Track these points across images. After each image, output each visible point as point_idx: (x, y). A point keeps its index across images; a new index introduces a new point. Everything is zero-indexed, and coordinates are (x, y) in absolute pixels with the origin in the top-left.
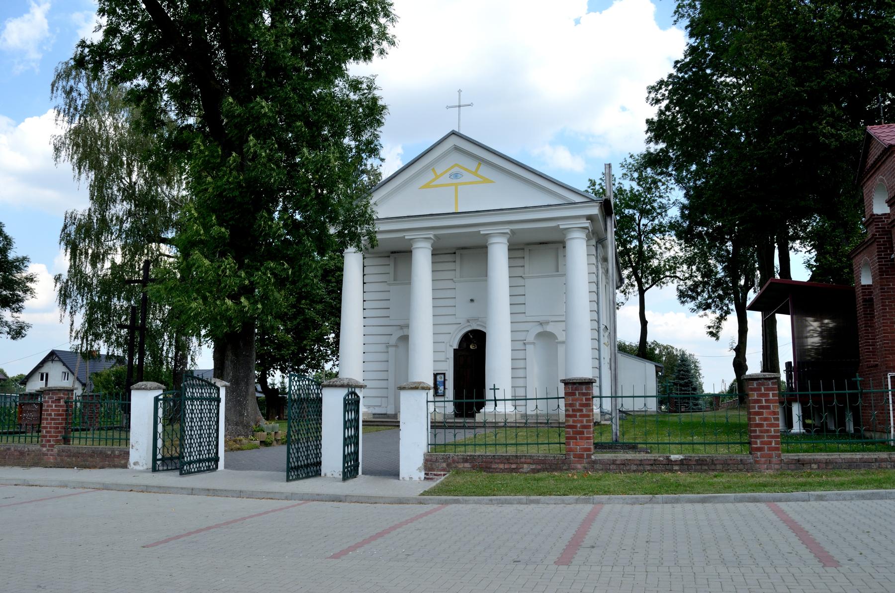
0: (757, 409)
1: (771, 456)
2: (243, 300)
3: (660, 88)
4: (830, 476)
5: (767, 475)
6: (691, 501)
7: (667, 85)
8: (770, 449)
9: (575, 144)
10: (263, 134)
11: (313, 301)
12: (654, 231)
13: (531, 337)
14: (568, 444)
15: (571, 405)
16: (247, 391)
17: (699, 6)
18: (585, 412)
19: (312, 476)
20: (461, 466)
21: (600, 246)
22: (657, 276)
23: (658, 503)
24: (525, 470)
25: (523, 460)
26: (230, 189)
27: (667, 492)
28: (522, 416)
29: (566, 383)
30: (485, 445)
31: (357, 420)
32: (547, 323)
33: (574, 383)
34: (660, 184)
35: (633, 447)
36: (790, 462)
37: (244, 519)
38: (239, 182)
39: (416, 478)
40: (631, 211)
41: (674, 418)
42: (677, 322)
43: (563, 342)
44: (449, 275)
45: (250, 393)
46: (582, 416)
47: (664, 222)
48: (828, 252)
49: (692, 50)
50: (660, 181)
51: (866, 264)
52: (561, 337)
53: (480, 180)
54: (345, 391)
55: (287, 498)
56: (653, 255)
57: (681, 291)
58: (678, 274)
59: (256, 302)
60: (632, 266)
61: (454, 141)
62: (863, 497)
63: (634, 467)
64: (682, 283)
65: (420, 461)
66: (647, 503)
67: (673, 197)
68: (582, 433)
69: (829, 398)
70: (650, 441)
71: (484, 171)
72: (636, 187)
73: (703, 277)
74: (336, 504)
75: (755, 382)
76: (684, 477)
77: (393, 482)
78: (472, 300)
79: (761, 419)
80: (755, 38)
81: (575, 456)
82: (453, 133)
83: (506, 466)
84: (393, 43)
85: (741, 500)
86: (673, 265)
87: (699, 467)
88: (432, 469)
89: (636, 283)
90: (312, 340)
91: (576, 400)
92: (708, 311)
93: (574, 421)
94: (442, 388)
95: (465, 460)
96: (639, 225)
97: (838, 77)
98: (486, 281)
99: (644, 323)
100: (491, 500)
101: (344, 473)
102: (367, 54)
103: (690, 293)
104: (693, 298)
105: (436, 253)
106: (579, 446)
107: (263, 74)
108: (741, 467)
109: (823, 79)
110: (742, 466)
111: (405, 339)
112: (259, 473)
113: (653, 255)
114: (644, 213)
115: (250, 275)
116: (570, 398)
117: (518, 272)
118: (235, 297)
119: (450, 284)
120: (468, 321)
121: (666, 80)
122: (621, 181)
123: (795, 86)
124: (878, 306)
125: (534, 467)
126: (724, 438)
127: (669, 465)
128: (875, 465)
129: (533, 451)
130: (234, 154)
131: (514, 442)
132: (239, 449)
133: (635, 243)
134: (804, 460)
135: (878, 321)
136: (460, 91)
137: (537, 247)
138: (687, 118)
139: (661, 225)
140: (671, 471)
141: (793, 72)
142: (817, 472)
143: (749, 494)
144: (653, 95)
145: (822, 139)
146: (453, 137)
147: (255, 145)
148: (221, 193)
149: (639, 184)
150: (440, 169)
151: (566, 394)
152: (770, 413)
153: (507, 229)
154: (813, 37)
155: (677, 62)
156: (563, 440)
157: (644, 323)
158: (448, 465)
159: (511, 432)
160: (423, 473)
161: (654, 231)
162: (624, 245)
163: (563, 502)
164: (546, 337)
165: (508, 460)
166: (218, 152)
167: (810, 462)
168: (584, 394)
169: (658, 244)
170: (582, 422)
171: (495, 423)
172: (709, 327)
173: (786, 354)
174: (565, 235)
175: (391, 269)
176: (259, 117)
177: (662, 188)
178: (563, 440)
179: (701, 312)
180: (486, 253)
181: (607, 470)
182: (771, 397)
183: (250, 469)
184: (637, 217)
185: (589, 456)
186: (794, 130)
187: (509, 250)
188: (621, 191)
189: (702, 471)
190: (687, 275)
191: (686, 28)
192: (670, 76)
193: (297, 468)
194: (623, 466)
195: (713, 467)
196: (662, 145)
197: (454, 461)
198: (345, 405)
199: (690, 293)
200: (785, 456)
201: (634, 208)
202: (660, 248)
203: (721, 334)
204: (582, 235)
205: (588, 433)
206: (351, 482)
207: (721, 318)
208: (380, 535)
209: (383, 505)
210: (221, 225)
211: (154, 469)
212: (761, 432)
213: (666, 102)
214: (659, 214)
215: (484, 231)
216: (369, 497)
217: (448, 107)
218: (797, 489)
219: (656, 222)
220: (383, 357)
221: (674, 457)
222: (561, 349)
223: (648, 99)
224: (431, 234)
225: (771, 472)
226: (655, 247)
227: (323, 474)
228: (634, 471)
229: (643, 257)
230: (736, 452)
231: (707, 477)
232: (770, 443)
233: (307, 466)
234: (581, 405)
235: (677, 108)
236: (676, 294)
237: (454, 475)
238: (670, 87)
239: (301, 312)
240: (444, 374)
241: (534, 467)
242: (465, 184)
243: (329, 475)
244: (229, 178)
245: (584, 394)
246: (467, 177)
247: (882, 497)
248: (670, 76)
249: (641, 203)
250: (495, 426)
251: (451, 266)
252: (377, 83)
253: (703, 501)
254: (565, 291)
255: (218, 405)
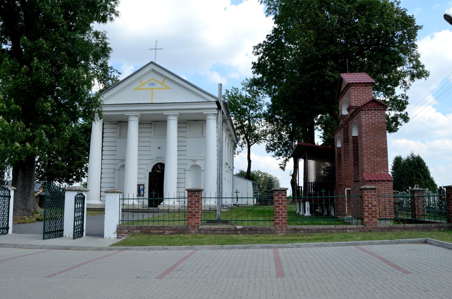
0: (277, 205)
1: (282, 227)
2: (27, 144)
3: (260, 47)
4: (324, 236)
5: (280, 236)
6: (239, 248)
7: (263, 46)
8: (283, 223)
9: (222, 70)
10: (41, 58)
11: (77, 145)
12: (256, 117)
13: (188, 167)
14: (188, 220)
15: (190, 202)
16: (30, 192)
17: (278, 9)
18: (197, 205)
19: (58, 237)
20: (135, 231)
21: (224, 123)
22: (257, 139)
23: (224, 249)
24: (166, 234)
25: (166, 228)
26: (22, 85)
27: (229, 244)
28: (182, 206)
29: (189, 191)
30: (158, 221)
31: (83, 208)
32: (197, 160)
33: (192, 191)
34: (260, 94)
35: (226, 222)
36: (291, 230)
37: (11, 259)
38: (28, 82)
39: (112, 238)
40: (245, 107)
41: (262, 208)
42: (267, 162)
43: (203, 170)
44: (148, 135)
45: (31, 193)
46: (195, 207)
47: (261, 113)
48: (329, 131)
49: (275, 30)
50: (260, 92)
51: (339, 138)
52: (203, 168)
53: (164, 87)
54: (76, 193)
55: (40, 248)
56: (255, 128)
57: (267, 147)
58: (267, 138)
59: (35, 146)
60: (245, 134)
61: (152, 66)
62: (317, 246)
63: (219, 232)
64: (269, 142)
65: (115, 229)
66: (219, 249)
67: (266, 100)
68: (195, 215)
69: (321, 200)
70: (239, 219)
71: (167, 83)
72: (248, 95)
73: (279, 140)
74: (65, 251)
75: (277, 192)
76: (241, 237)
77: (100, 239)
78: (159, 148)
79: (279, 209)
80: (300, 27)
81: (192, 226)
82: (152, 63)
83: (158, 232)
84: (117, 15)
85: (262, 248)
86: (265, 134)
87: (249, 232)
88: (120, 233)
89: (246, 142)
90: (76, 166)
91: (193, 199)
92: (281, 157)
93: (192, 210)
94: (142, 192)
95: (137, 229)
96: (249, 113)
97: (335, 49)
98: (166, 138)
99: (250, 161)
100: (144, 248)
101: (74, 235)
102: (104, 20)
103: (272, 148)
104: (273, 150)
105: (141, 123)
106: (193, 222)
107: (44, 26)
108: (269, 232)
109: (329, 49)
110: (269, 231)
111: (123, 166)
112: (30, 235)
113: (255, 128)
114: (252, 108)
115: (33, 131)
116: (190, 198)
117: (183, 134)
118: (23, 143)
119: (148, 139)
120: (157, 158)
121: (262, 43)
122: (241, 91)
123: (316, 52)
124: (343, 157)
125: (171, 232)
126: (268, 218)
127: (236, 231)
128: (328, 231)
129: (171, 224)
130: (25, 66)
131: (178, 219)
132: (23, 223)
133: (247, 122)
134: (297, 229)
135: (343, 165)
136: (156, 41)
137: (192, 122)
138: (272, 62)
139: (260, 114)
140: (237, 234)
141: (316, 45)
142: (303, 234)
143: (267, 245)
144: (256, 50)
145: (327, 78)
146: (151, 65)
147: (37, 62)
148: (17, 87)
149: (250, 93)
150: (145, 80)
151: (188, 196)
152: (283, 207)
153: (177, 113)
154: (325, 29)
155: (268, 36)
156: (186, 219)
157: (250, 161)
158: (129, 231)
159: (171, 215)
160: (116, 235)
161: (256, 117)
162: (241, 123)
163: (180, 249)
164: (196, 167)
165: (159, 228)
166: (17, 65)
167: (300, 230)
168: (197, 196)
169: (259, 123)
170: (195, 210)
171: (163, 210)
172: (280, 165)
173: (312, 178)
174: (206, 117)
175: (118, 130)
176: (41, 48)
177: (261, 96)
178: (186, 219)
179: (277, 157)
180: (167, 124)
181: (206, 233)
182: (284, 199)
183: (27, 233)
184: (248, 109)
185: (198, 227)
186: (315, 73)
187: (178, 123)
188: (241, 96)
189: (250, 234)
190: (272, 139)
191: (273, 19)
192: (264, 42)
193: (49, 233)
194: (214, 231)
195: (256, 232)
196: (260, 76)
197: (132, 229)
198: (76, 200)
199: (272, 148)
200: (290, 227)
201: (246, 105)
202: (259, 125)
203: (286, 168)
204: (214, 117)
205: (198, 215)
206: (77, 240)
207: (286, 160)
208: (79, 266)
209: (90, 251)
210: (16, 104)
211: (74, 238)
212: (279, 215)
213: (261, 54)
214: (259, 108)
215: (165, 113)
216: (83, 247)
217: (150, 49)
218: (289, 242)
219: (258, 112)
220: (112, 175)
221: (238, 227)
222: (202, 173)
223: (253, 52)
224: (138, 113)
225: (282, 234)
226: (256, 125)
227: (64, 236)
228: (219, 234)
229: (251, 129)
230: (268, 225)
231: (252, 237)
232: (283, 220)
233: (55, 231)
234: (195, 202)
235: (267, 58)
236: (265, 147)
237: (131, 236)
238: (264, 47)
239: (70, 151)
240: (144, 185)
241: (171, 232)
242: (157, 89)
243: (67, 236)
244: (22, 79)
245: (197, 196)
246: (158, 85)
247: (325, 246)
248: (264, 42)
249: (251, 103)
250: (168, 211)
251: (149, 130)
252: (107, 36)
253: (245, 248)
254: (204, 146)
255: (9, 200)
